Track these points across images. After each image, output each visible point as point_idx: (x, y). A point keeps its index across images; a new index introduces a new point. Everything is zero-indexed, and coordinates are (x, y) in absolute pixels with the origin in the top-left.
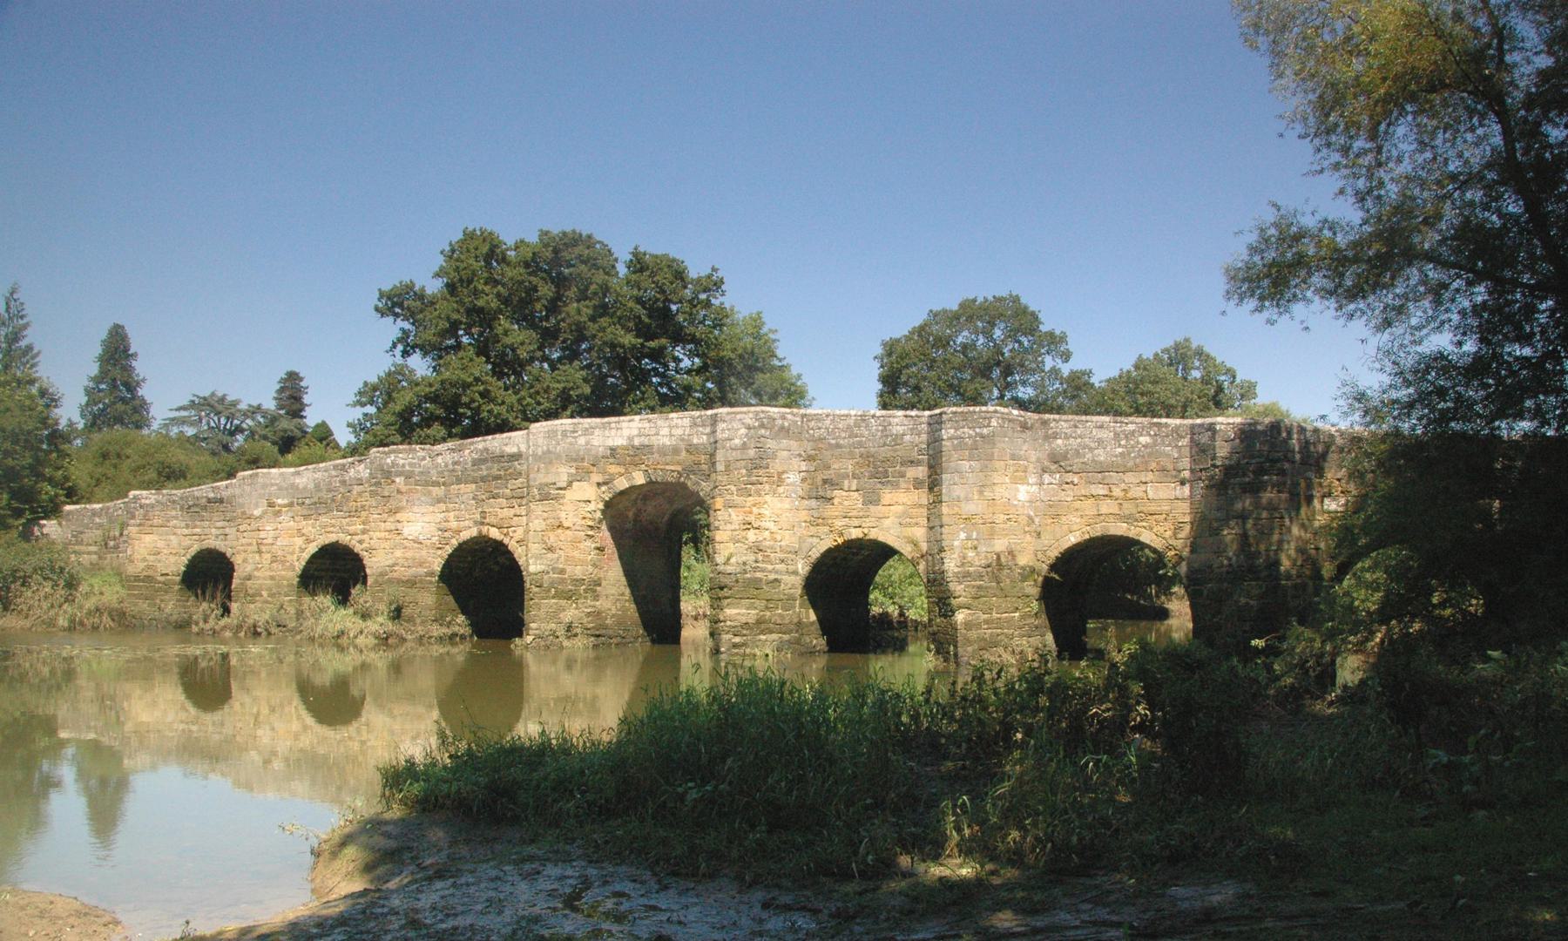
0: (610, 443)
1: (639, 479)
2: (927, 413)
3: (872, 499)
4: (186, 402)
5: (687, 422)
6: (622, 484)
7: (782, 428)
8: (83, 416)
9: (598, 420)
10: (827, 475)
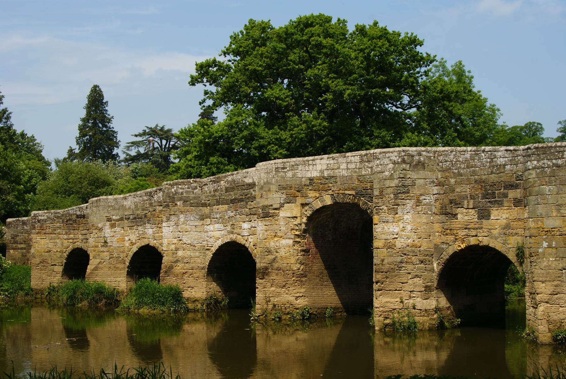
0: (309, 175)
1: (328, 201)
2: (522, 147)
3: (484, 215)
4: (141, 132)
5: (357, 159)
6: (318, 205)
7: (419, 162)
8: (78, 143)
9: (301, 159)
10: (451, 196)
